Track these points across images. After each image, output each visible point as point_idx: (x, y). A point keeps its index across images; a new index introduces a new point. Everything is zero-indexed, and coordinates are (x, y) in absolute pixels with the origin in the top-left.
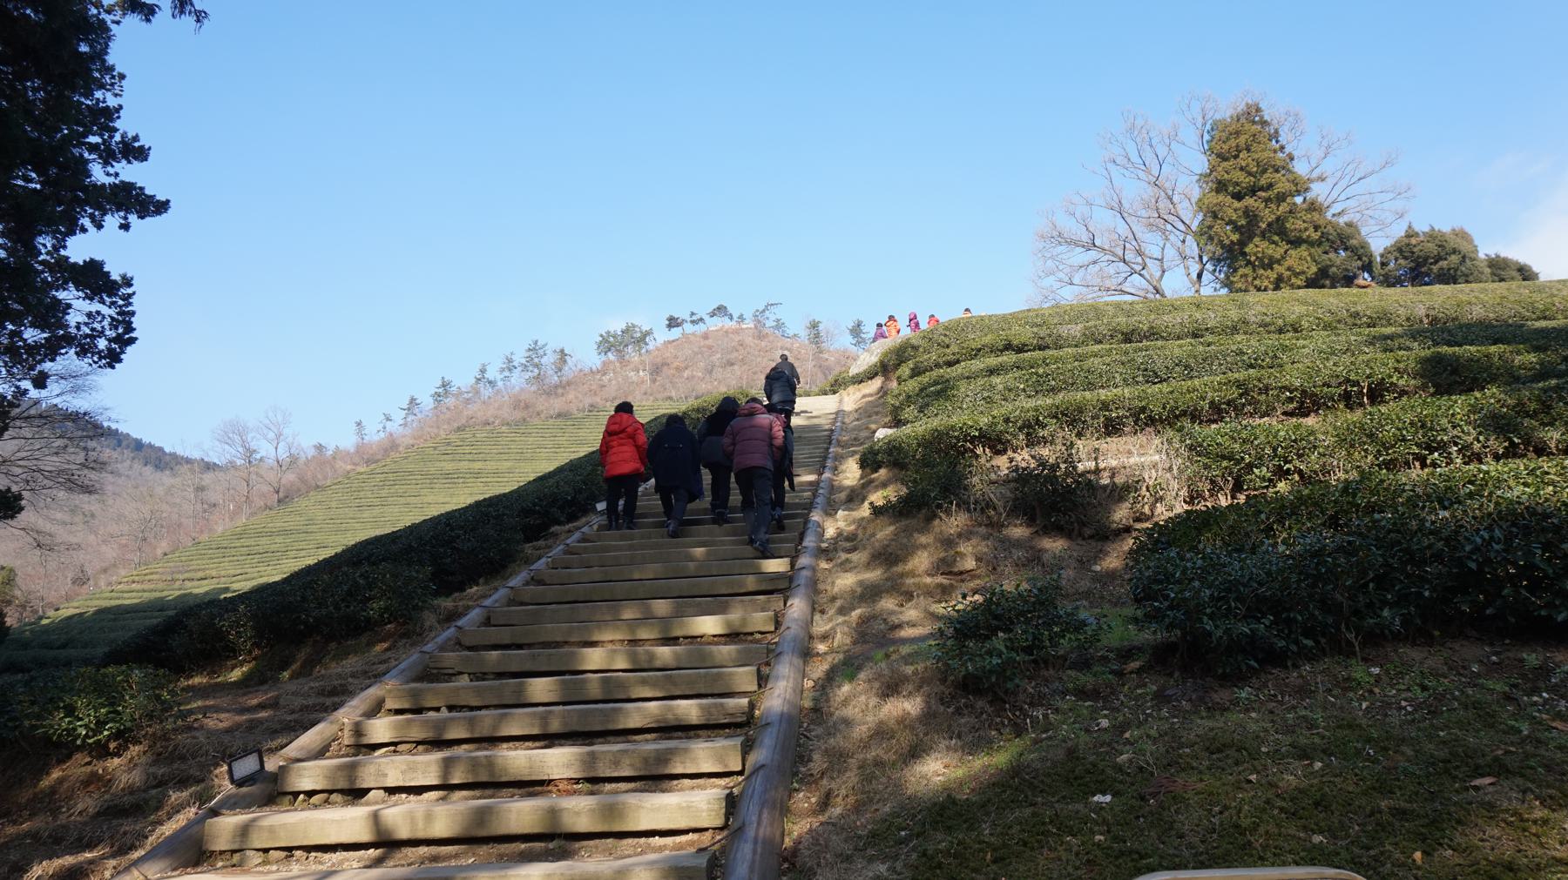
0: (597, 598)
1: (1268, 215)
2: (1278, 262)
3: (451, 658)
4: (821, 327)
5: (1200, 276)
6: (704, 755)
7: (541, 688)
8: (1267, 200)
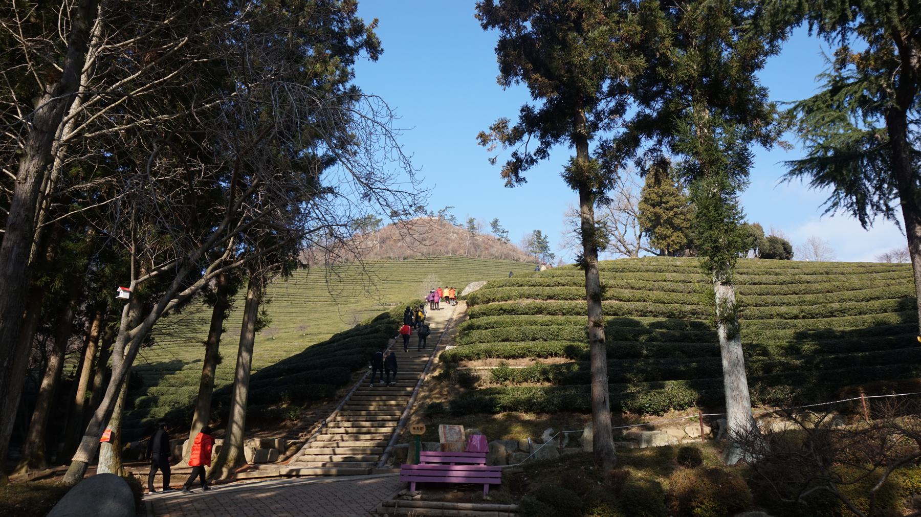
0: (370, 397)
1: (665, 216)
2: (669, 237)
3: (346, 407)
4: (475, 222)
5: (640, 236)
6: (391, 424)
7: (363, 413)
8: (667, 209)
